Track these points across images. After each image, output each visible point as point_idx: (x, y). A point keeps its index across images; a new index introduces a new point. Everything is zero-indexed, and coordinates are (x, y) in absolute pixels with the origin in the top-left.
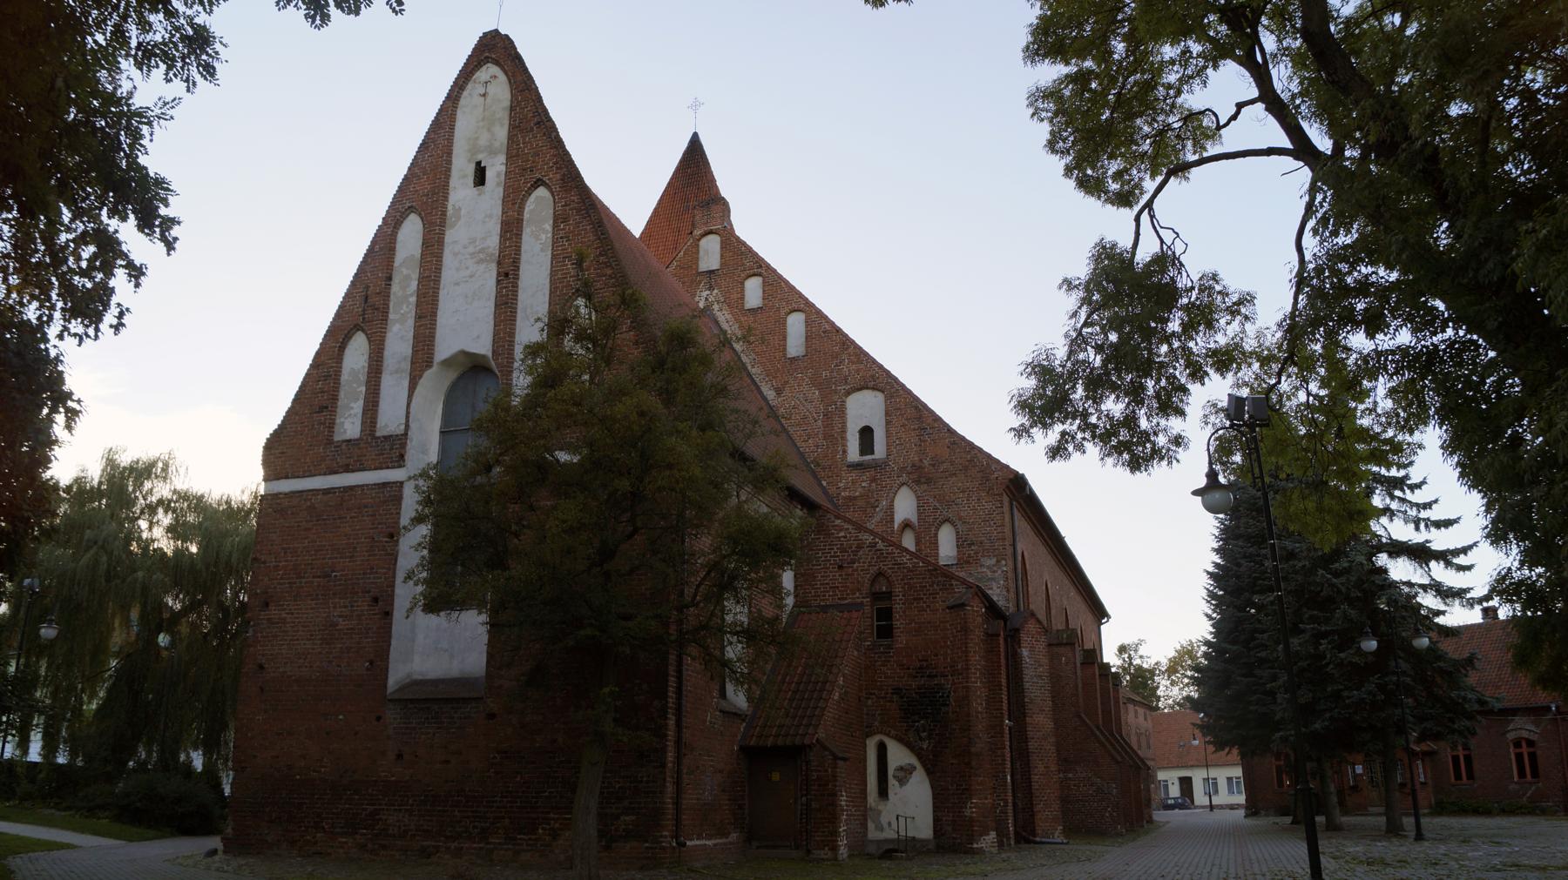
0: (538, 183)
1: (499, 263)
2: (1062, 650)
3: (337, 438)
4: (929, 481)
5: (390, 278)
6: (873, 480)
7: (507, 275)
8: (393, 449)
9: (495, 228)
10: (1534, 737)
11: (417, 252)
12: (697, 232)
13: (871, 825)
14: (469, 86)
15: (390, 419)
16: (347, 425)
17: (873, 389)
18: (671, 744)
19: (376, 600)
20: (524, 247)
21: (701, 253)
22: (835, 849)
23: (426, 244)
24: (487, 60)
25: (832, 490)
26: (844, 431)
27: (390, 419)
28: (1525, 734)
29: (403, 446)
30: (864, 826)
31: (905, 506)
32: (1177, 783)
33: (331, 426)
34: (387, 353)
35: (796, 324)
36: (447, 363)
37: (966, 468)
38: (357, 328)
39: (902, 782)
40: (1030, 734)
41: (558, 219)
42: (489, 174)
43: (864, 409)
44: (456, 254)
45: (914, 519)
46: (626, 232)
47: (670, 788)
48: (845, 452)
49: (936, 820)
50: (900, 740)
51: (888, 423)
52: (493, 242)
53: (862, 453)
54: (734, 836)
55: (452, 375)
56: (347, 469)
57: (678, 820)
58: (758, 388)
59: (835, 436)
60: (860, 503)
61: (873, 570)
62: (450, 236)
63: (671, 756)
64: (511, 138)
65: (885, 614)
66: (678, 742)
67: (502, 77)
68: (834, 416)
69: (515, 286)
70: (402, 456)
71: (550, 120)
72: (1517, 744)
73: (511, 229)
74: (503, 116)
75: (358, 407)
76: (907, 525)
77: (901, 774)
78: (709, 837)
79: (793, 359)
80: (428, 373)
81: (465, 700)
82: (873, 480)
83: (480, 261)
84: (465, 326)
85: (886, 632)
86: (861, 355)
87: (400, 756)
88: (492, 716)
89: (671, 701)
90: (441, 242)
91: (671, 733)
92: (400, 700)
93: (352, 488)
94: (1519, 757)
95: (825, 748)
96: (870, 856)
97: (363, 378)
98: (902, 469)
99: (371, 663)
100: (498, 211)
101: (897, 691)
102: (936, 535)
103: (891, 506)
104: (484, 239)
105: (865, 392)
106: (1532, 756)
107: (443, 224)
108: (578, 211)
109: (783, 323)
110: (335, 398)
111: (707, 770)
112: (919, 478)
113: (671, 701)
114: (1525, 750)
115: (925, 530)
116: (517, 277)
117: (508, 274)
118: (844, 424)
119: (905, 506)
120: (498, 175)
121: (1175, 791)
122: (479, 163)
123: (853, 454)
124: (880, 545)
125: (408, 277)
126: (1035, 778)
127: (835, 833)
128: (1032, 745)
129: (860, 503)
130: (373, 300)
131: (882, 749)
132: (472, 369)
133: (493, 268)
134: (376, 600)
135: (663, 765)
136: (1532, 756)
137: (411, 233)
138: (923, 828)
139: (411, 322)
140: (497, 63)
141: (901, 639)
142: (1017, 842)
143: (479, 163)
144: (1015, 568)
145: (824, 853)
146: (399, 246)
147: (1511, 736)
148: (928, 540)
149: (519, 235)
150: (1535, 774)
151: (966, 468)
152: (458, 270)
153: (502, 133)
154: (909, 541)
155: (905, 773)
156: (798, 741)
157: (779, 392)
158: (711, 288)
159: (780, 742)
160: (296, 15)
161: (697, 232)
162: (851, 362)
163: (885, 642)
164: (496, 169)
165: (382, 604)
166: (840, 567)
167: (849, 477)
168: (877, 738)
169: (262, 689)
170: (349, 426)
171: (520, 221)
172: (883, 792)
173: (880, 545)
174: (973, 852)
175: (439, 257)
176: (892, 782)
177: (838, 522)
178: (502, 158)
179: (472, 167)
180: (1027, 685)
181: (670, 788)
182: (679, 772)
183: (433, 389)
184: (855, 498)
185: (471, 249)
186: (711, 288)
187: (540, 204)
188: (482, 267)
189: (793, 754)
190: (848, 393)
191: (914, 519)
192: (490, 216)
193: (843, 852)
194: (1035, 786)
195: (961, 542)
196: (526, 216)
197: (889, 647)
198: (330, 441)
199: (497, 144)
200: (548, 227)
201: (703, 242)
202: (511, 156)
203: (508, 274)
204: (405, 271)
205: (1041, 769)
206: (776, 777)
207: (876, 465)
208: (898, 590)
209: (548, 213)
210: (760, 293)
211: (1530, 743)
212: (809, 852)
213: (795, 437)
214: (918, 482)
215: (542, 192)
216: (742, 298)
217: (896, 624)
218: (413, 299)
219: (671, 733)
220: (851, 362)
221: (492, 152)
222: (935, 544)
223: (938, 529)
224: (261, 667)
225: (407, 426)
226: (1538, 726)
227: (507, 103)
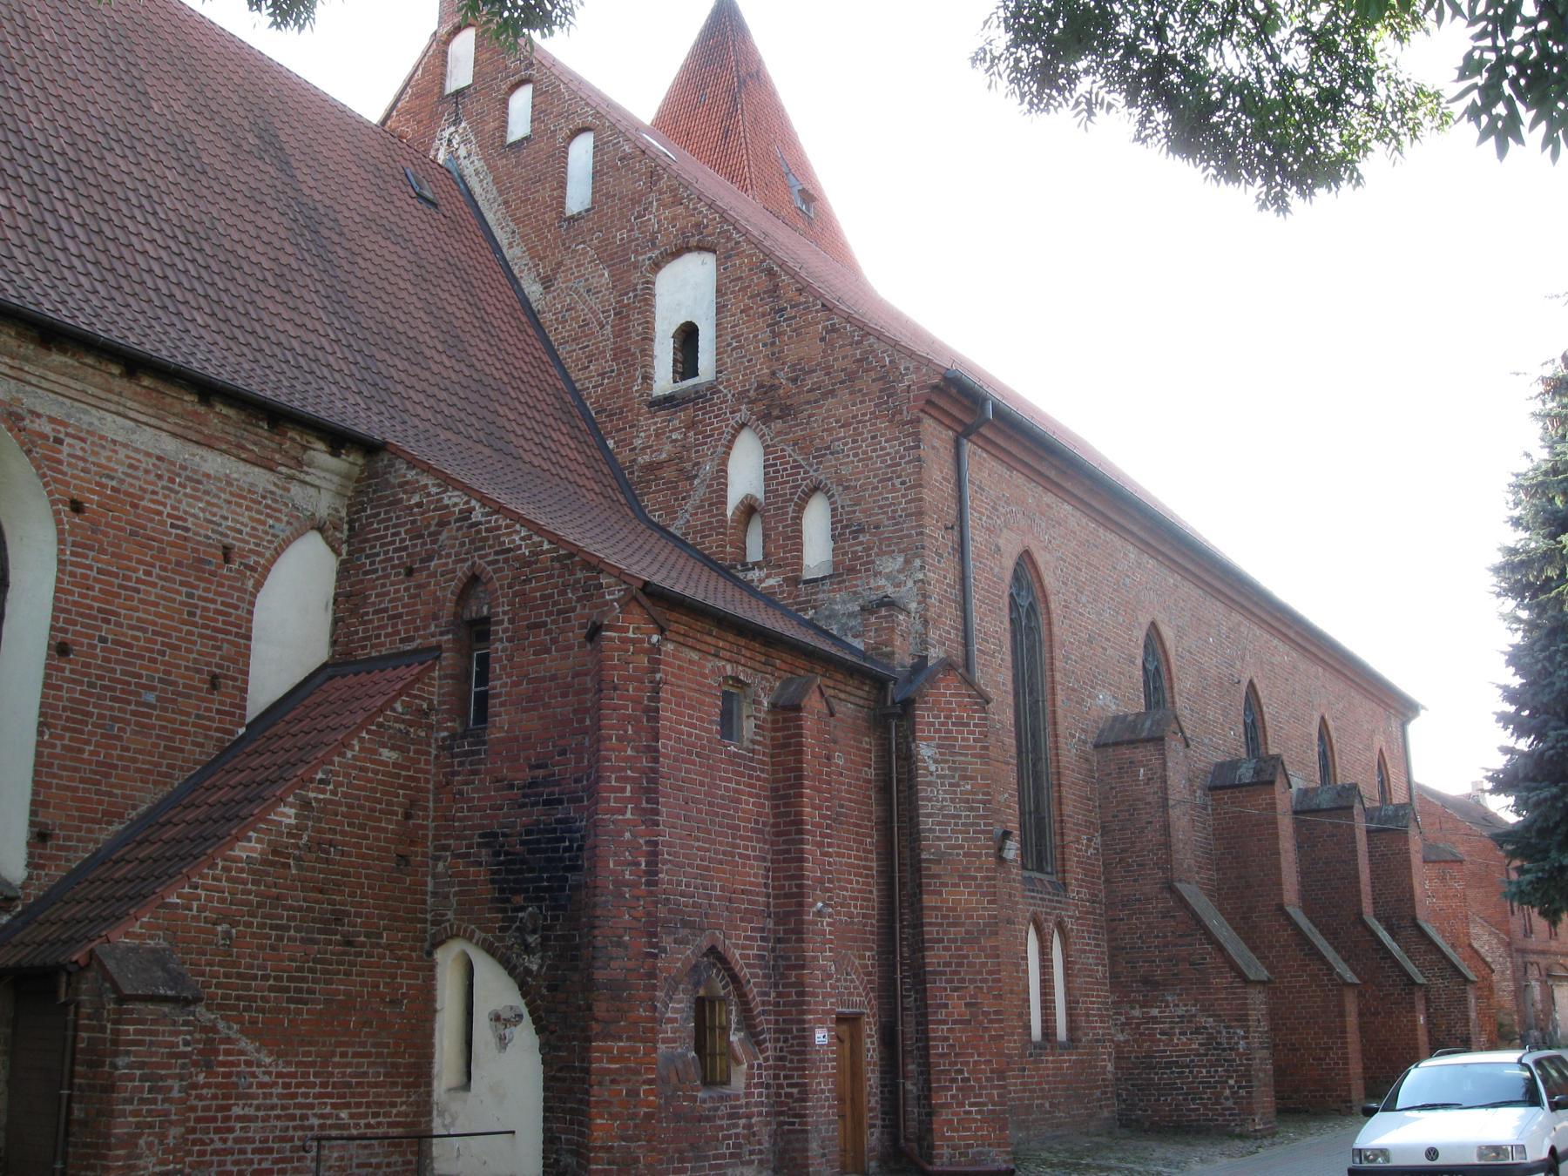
2: (1140, 753)
4: (786, 412)
6: (691, 425)
25: (623, 456)
26: (648, 338)
31: (745, 472)
35: (581, 153)
37: (852, 377)
40: (931, 932)
51: (720, 309)
60: (669, 473)
61: (462, 570)
76: (749, 509)
82: (691, 425)
98: (741, 396)
101: (489, 837)
102: (798, 519)
103: (722, 473)
112: (771, 407)
118: (649, 325)
119: (745, 472)
123: (663, 380)
126: (938, 1031)
128: (934, 958)
141: (502, 720)
151: (852, 377)
157: (547, 283)
160: (1556, 369)
162: (662, 204)
166: (410, 572)
167: (650, 423)
177: (411, 475)
180: (927, 823)
184: (659, 465)
186: (456, 122)
190: (657, 266)
195: (841, 530)
205: (958, 1006)
213: (569, 363)
214: (766, 418)
220: (662, 204)
222: (795, 538)
223: (800, 508)
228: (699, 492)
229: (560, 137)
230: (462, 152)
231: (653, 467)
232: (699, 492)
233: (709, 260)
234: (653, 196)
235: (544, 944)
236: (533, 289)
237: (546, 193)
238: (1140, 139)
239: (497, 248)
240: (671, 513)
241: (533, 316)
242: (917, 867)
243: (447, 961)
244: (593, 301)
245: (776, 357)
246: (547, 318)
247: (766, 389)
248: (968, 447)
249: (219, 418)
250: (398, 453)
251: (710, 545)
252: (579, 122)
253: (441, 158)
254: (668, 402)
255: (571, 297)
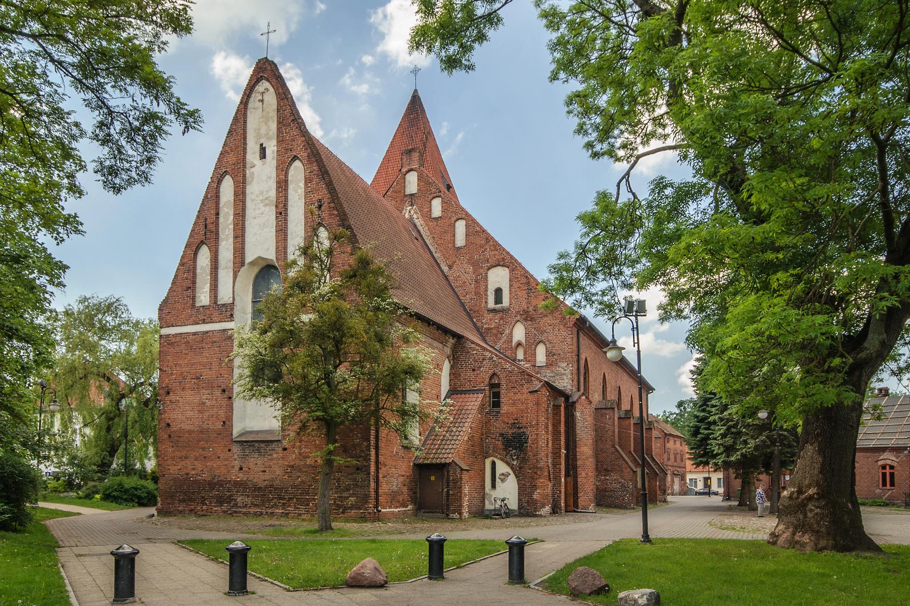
0: (295, 158)
1: (276, 207)
2: (607, 412)
3: (198, 305)
4: (532, 319)
5: (218, 214)
6: (502, 318)
7: (281, 213)
8: (227, 311)
9: (273, 186)
10: (895, 464)
11: (232, 198)
12: (404, 170)
13: (487, 502)
14: (253, 95)
15: (225, 296)
16: (202, 298)
17: (503, 266)
18: (373, 464)
19: (224, 391)
20: (290, 197)
21: (407, 183)
22: (460, 514)
23: (236, 194)
24: (262, 78)
25: (479, 324)
27: (225, 296)
28: (889, 462)
29: (232, 309)
30: (483, 502)
31: (519, 333)
32: (702, 480)
33: (194, 298)
34: (220, 258)
36: (252, 263)
38: (202, 243)
39: (503, 481)
40: (578, 457)
41: (308, 181)
42: (268, 152)
43: (499, 277)
44: (253, 200)
45: (523, 341)
46: (353, 178)
47: (373, 485)
48: (486, 302)
49: (520, 500)
50: (502, 460)
51: (511, 286)
52: (273, 193)
53: (496, 303)
54: (410, 507)
55: (256, 270)
56: (204, 322)
57: (377, 499)
58: (438, 265)
59: (480, 294)
60: (494, 331)
61: (491, 372)
62: (249, 189)
63: (373, 469)
64: (279, 129)
65: (497, 395)
66: (377, 462)
67: (272, 90)
68: (481, 280)
69: (286, 220)
70: (232, 315)
71: (300, 118)
72: (884, 467)
73: (282, 185)
74: (274, 115)
75: (207, 288)
76: (519, 344)
77: (502, 477)
78: (396, 507)
79: (459, 248)
80: (242, 269)
81: (272, 442)
82: (502, 318)
83: (266, 205)
84: (261, 244)
85: (497, 404)
86: (497, 246)
87: (241, 469)
88: (285, 449)
89: (372, 442)
90: (244, 193)
91: (373, 458)
92: (240, 441)
93: (207, 332)
94: (884, 475)
95: (457, 465)
96: (487, 517)
97: (208, 271)
99: (224, 422)
100: (274, 175)
101: (502, 435)
104: (268, 192)
105: (499, 268)
106: (892, 475)
107: (244, 182)
108: (318, 176)
109: (454, 226)
110: (194, 283)
111: (394, 475)
112: (527, 317)
113: (372, 442)
114: (888, 471)
115: (530, 346)
116: (286, 215)
117: (282, 212)
118: (487, 286)
120: (273, 152)
121: (700, 486)
122: (261, 145)
123: (491, 304)
124: (495, 358)
125: (228, 214)
126: (579, 480)
127: (461, 506)
128: (579, 463)
129: (494, 331)
130: (210, 226)
131: (493, 464)
132: (266, 271)
133: (274, 208)
134: (224, 391)
135: (369, 474)
136: (892, 475)
137: (227, 187)
138: (513, 504)
139: (231, 240)
140: (268, 80)
141: (504, 409)
142: (566, 512)
143: (261, 145)
144: (578, 369)
145: (456, 516)
146: (221, 195)
147: (880, 463)
148: (530, 355)
149: (286, 190)
150: (892, 484)
152: (255, 210)
153: (274, 126)
154: (520, 355)
155: (505, 476)
156: (443, 461)
157: (450, 267)
158: (412, 205)
159: (434, 461)
161: (404, 170)
163: (496, 409)
164: (272, 149)
165: (227, 392)
168: (491, 459)
169: (170, 436)
170: (203, 298)
171: (286, 181)
172: (494, 486)
173: (495, 358)
174: (536, 516)
175: (244, 202)
176: (498, 480)
177: (473, 346)
178: (274, 142)
179: (259, 146)
180: (578, 432)
181: (373, 485)
182: (377, 477)
183: (247, 277)
185: (261, 198)
187: (297, 172)
188: (268, 208)
189: (441, 468)
191: (523, 341)
192: (270, 178)
193: (466, 515)
194: (579, 483)
195: (549, 354)
196: (290, 178)
197: (498, 412)
198: (193, 306)
199: (271, 133)
200: (302, 185)
201: (407, 176)
202: (280, 141)
203: (282, 212)
204: (226, 210)
205: (583, 474)
206: (433, 478)
207: (503, 310)
208: (503, 382)
209: (301, 176)
210: (440, 208)
211: (892, 467)
212: (448, 515)
214: (526, 320)
215: (297, 163)
216: (430, 211)
217: (502, 400)
218: (232, 227)
219: (373, 458)
221: (269, 139)
224: (168, 425)
225: (234, 298)
226: (897, 458)
227: (275, 107)
228: (504, 339)
229: (453, 219)
230: (415, 216)
231: (489, 329)
232: (504, 339)
233: (507, 270)
234: (488, 247)
235: (517, 459)
236: (445, 269)
237: (448, 237)
238: (470, 67)
239: (431, 253)
240: (495, 343)
241: (446, 277)
242: (575, 442)
243: (488, 462)
244: (467, 276)
245: (529, 303)
246: (451, 278)
247: (526, 312)
248: (581, 335)
249: (432, 329)
250: (467, 339)
251: (508, 353)
252: (460, 216)
253: (407, 216)
254: (494, 311)
255: (463, 273)
